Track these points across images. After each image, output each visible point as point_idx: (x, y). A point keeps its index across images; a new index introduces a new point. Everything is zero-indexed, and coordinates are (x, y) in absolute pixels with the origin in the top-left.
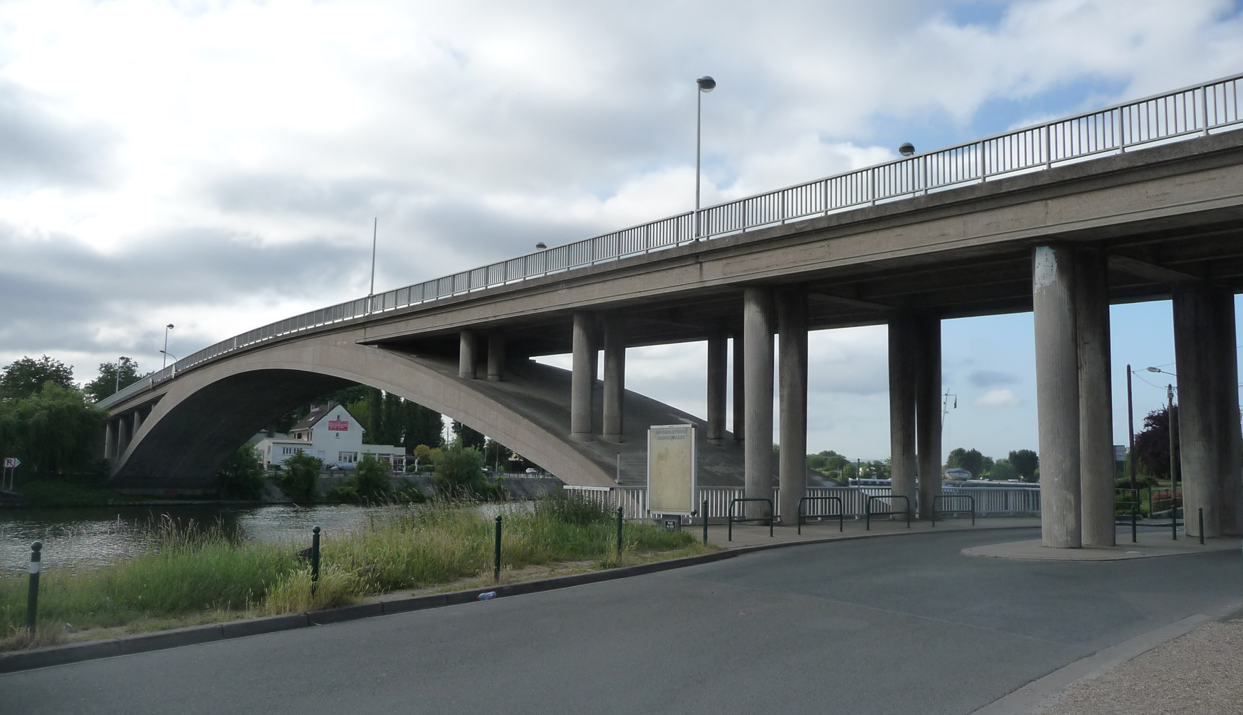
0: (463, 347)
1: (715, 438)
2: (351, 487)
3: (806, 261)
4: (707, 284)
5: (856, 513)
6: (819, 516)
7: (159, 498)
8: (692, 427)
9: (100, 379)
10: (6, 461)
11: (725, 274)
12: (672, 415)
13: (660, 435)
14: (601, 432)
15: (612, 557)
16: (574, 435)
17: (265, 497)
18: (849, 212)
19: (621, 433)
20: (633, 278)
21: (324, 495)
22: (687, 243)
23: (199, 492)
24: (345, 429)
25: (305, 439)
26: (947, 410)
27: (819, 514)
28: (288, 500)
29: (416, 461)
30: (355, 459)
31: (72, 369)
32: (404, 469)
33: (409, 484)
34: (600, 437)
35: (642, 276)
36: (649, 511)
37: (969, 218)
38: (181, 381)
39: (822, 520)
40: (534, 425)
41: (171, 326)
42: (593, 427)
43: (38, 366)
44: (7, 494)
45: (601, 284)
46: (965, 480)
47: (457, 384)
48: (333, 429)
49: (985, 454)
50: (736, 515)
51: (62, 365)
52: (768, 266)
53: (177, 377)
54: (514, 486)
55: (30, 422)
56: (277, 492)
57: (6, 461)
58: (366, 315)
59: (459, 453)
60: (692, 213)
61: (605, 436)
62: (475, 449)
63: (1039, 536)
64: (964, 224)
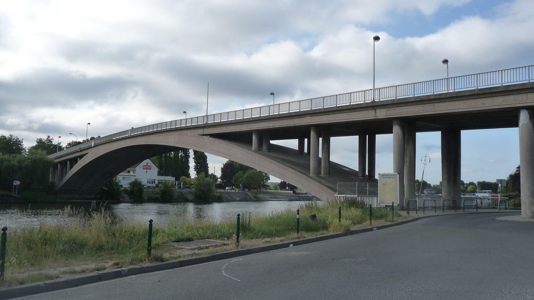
0: (254, 138)
1: (362, 176)
2: (158, 195)
3: (423, 110)
4: (378, 118)
5: (417, 206)
6: (430, 207)
7: (78, 199)
8: (398, 174)
9: (36, 145)
10: (14, 182)
11: (387, 114)
12: (338, 166)
13: (383, 177)
14: (321, 174)
15: (390, 218)
16: (311, 175)
17: (122, 199)
18: (444, 93)
19: (329, 174)
20: (343, 114)
21: (146, 198)
22: (370, 101)
23: (93, 197)
24: (150, 169)
25: (132, 173)
26: (426, 163)
27: (430, 206)
28: (131, 200)
29: (182, 184)
30: (154, 183)
31: (23, 141)
32: (177, 187)
33: (182, 194)
34: (320, 175)
35: (347, 113)
36: (379, 204)
37: (495, 98)
38: (97, 148)
39: (431, 209)
40: (294, 171)
41: (89, 124)
42: (318, 173)
43: (8, 139)
44: (15, 197)
45: (328, 115)
46: (433, 194)
47: (252, 152)
48: (145, 169)
49: (428, 183)
50: (375, 207)
51: (18, 139)
52: (406, 112)
53: (94, 146)
54: (226, 195)
55: (24, 165)
56: (127, 197)
57: (14, 182)
58: (204, 123)
59: (204, 180)
60: (372, 89)
61: (322, 175)
62: (210, 178)
63: (521, 214)
64: (493, 100)
